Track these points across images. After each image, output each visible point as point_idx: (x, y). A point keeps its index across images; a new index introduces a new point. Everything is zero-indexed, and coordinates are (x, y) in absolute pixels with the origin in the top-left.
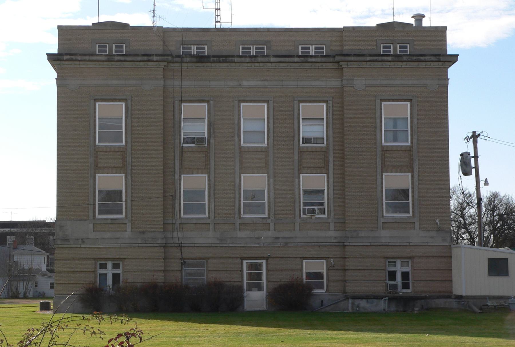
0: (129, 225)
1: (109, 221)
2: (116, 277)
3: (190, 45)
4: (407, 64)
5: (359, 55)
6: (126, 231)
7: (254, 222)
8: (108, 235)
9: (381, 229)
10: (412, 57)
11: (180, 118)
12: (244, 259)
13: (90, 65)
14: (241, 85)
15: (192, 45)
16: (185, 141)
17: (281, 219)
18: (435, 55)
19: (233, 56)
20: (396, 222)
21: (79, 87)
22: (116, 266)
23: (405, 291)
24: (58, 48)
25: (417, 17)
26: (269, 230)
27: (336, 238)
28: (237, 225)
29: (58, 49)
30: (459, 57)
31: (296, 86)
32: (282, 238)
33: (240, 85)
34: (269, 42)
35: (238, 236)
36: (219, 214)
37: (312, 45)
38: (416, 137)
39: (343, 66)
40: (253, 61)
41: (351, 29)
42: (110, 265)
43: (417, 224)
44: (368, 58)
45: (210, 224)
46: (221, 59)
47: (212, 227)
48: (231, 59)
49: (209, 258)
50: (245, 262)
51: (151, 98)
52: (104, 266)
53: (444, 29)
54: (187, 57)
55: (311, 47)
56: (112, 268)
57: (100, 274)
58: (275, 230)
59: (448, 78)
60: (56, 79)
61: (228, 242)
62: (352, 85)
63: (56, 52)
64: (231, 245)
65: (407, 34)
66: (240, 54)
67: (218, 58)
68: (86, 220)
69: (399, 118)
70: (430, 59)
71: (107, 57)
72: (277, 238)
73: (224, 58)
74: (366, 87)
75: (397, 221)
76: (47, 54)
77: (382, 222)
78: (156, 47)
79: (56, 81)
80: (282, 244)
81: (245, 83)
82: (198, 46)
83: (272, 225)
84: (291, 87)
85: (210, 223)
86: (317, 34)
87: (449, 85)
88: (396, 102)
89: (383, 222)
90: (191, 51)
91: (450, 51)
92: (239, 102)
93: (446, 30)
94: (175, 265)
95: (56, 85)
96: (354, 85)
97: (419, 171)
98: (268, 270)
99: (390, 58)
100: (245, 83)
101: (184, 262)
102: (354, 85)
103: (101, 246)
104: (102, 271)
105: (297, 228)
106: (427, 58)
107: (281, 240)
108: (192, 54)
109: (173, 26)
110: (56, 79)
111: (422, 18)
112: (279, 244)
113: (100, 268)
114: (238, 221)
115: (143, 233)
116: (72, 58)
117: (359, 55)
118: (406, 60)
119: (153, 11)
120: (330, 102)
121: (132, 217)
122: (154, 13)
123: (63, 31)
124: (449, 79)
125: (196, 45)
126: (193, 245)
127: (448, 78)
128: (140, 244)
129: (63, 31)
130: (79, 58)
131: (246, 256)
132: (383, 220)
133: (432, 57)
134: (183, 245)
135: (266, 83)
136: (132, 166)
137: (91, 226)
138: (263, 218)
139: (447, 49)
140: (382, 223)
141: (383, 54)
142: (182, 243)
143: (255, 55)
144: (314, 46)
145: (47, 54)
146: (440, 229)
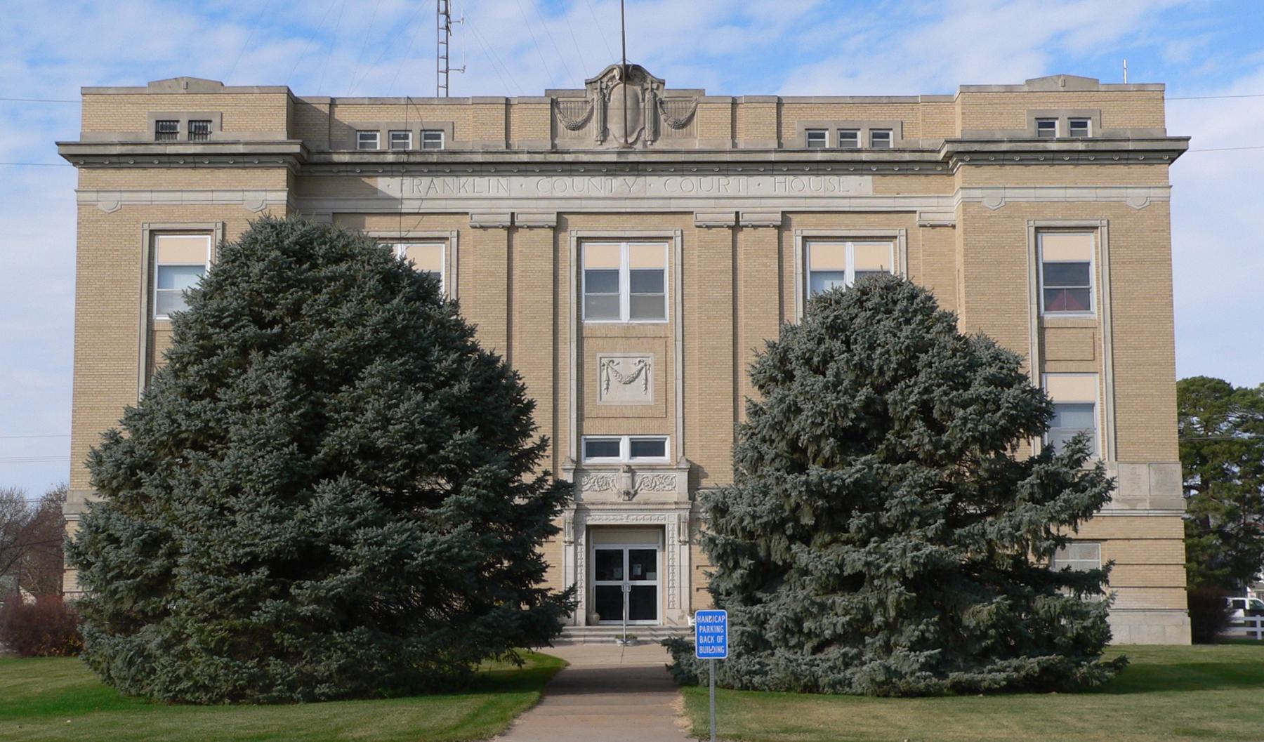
116: (1045, 147)
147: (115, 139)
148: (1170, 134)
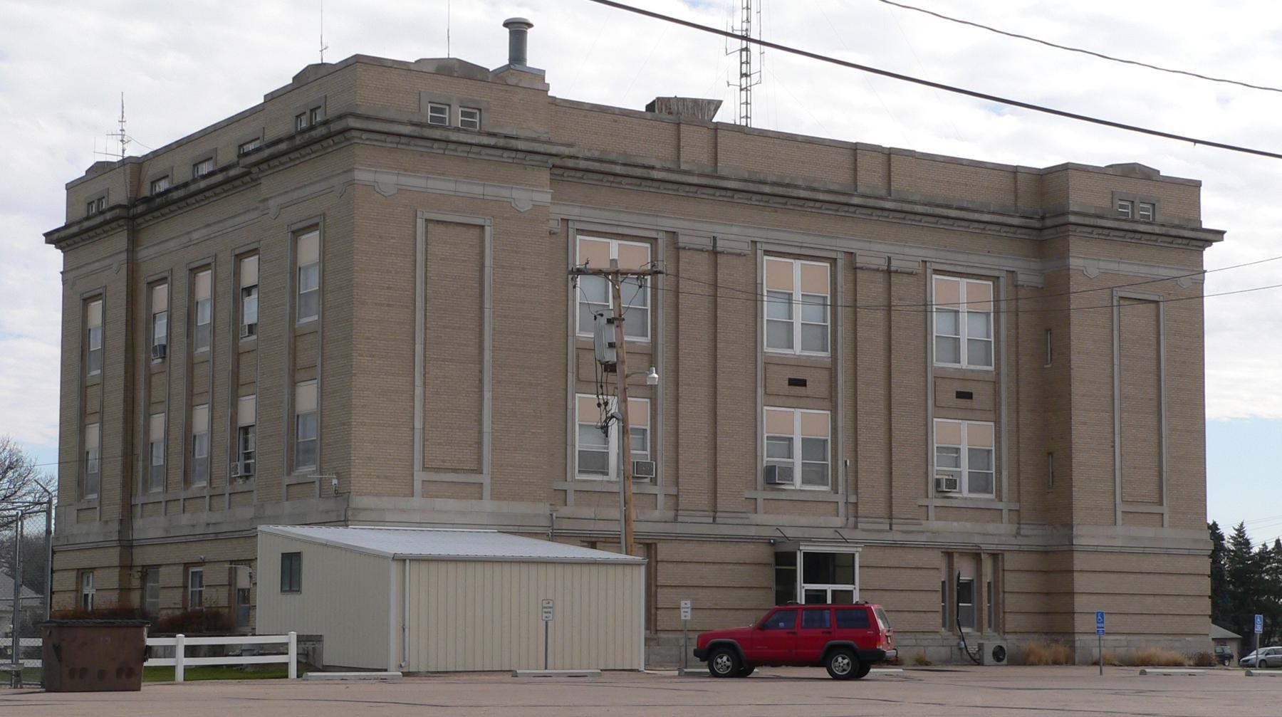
4: (480, 151)
30: (1225, 235)
49: (160, 566)
53: (1198, 184)
59: (1205, 269)
60: (62, 273)
77: (287, 485)
79: (61, 275)
87: (1205, 281)
91: (1207, 224)
93: (1201, 185)
124: (1205, 271)
127: (1205, 269)
132: (287, 481)
139: (1202, 219)
147: (405, 118)
148: (1204, 226)
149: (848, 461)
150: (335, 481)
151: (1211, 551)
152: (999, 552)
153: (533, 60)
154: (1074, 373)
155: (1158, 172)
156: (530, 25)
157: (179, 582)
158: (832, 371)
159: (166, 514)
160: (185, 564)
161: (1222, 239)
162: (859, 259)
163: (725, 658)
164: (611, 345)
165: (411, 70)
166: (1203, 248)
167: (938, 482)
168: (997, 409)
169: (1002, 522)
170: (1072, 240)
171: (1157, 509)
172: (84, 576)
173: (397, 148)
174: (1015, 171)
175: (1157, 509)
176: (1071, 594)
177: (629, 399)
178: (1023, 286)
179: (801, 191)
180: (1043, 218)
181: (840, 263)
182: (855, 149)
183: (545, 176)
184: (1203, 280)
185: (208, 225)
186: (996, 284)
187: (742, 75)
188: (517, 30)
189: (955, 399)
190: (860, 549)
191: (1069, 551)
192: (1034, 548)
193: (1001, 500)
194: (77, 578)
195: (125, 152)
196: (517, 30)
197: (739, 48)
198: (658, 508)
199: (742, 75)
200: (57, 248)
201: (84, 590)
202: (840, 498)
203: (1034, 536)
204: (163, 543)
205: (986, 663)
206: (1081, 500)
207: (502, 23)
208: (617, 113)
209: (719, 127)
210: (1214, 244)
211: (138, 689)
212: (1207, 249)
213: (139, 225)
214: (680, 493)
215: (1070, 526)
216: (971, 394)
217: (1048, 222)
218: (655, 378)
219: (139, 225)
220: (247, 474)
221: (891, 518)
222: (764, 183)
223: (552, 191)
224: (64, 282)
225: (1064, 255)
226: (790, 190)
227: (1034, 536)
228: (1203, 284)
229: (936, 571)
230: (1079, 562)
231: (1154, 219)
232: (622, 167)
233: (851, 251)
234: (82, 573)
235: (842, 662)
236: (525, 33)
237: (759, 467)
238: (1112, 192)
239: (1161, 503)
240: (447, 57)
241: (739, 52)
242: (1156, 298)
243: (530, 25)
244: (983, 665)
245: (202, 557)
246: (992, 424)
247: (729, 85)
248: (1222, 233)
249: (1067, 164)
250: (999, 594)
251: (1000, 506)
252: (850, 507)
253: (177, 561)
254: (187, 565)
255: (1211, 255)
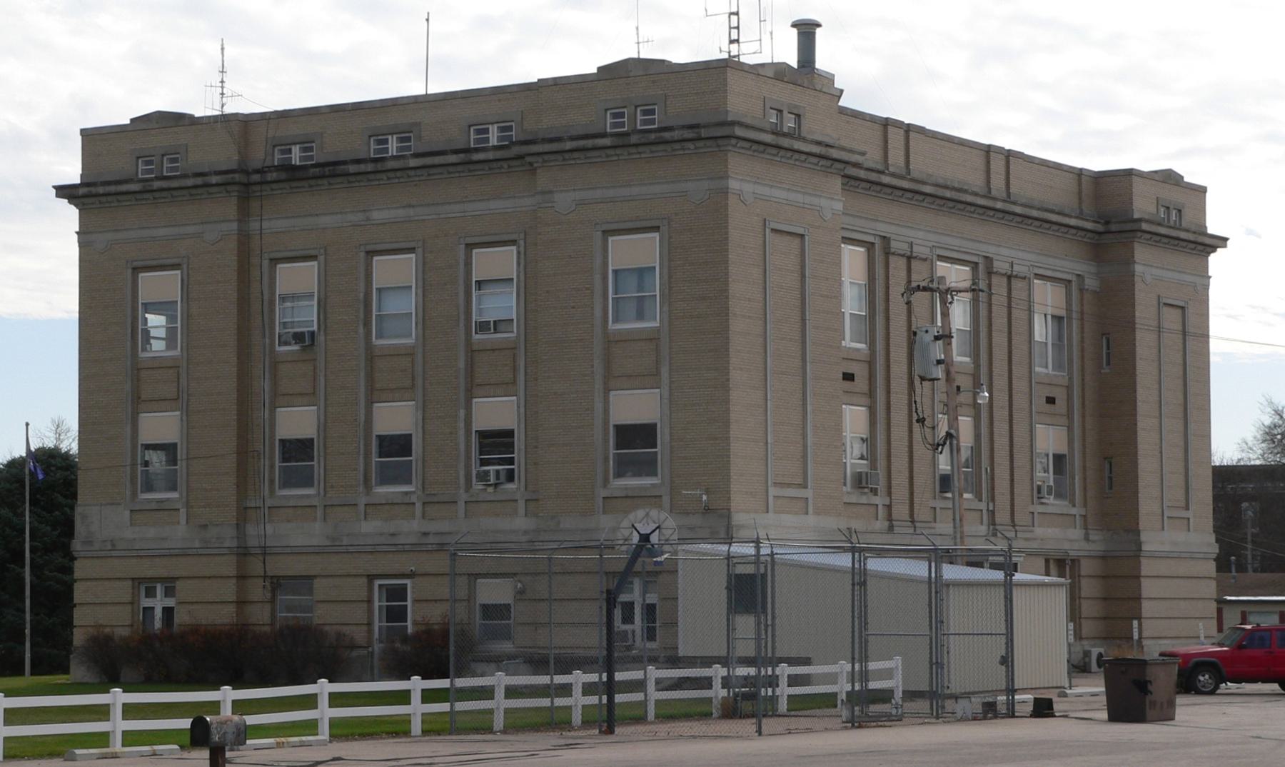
0: (183, 511)
1: (154, 506)
2: (168, 612)
3: (290, 144)
5: (551, 140)
6: (178, 523)
7: (390, 502)
8: (151, 532)
9: (601, 513)
10: (646, 135)
11: (273, 292)
12: (374, 579)
13: (124, 201)
14: (370, 220)
15: (390, 134)
16: (282, 340)
17: (434, 494)
18: (691, 127)
19: (344, 163)
20: (627, 497)
21: (710, 194)
22: (169, 592)
23: (650, 645)
24: (80, 172)
25: (804, 27)
26: (413, 516)
27: (526, 532)
28: (362, 508)
29: (82, 176)
30: (1228, 242)
31: (463, 214)
32: (434, 534)
33: (368, 219)
34: (418, 124)
35: (362, 531)
36: (332, 487)
37: (492, 124)
38: (871, 296)
39: (535, 165)
40: (380, 169)
41: (550, 83)
42: (159, 589)
43: (666, 500)
44: (569, 145)
45: (315, 506)
46: (327, 169)
47: (319, 512)
48: (342, 167)
49: (315, 577)
50: (377, 582)
51: (218, 259)
52: (150, 593)
54: (271, 172)
55: (490, 127)
56: (163, 595)
57: (144, 608)
58: (423, 517)
60: (77, 233)
61: (344, 543)
62: (550, 205)
63: (78, 181)
64: (351, 549)
65: (654, 82)
66: (470, 146)
67: (321, 169)
68: (119, 504)
69: (150, 303)
70: (682, 135)
71: (142, 184)
72: (425, 534)
73: (331, 168)
74: (576, 205)
75: (630, 495)
76: (54, 187)
77: (604, 498)
78: (223, 155)
79: (76, 236)
80: (434, 546)
81: (377, 215)
82: (302, 146)
83: (419, 506)
84: (454, 215)
85: (318, 504)
86: (499, 100)
88: (633, 234)
89: (604, 496)
90: (487, 136)
91: (1211, 230)
92: (604, 235)
94: (257, 591)
95: (77, 244)
96: (554, 204)
97: (671, 382)
98: (370, 601)
99: (606, 142)
100: (377, 215)
101: (276, 584)
102: (554, 204)
103: (142, 553)
104: (147, 603)
105: (522, 511)
106: (676, 134)
107: (431, 539)
108: (293, 163)
109: (214, 111)
110: (77, 233)
111: (815, 29)
112: (430, 547)
113: (146, 597)
114: (363, 500)
115: (205, 527)
116: (91, 192)
117: (551, 140)
118: (638, 142)
119: (220, 85)
120: (522, 243)
121: (188, 495)
122: (222, 87)
123: (93, 139)
125: (396, 133)
126: (288, 550)
128: (198, 550)
129: (93, 139)
130: (101, 190)
131: (379, 572)
132: (604, 493)
133: (685, 132)
134: (268, 551)
135: (411, 212)
136: (188, 395)
137: (127, 513)
138: (406, 493)
140: (601, 499)
141: (376, 156)
142: (265, 547)
143: (395, 154)
144: (496, 126)
145: (54, 187)
146: (709, 509)
149: (989, 469)
150: (705, 497)
151: (1216, 555)
152: (1076, 558)
153: (823, 62)
154: (1138, 379)
155: (1182, 177)
156: (819, 25)
157: (363, 594)
158: (871, 363)
159: (325, 519)
160: (368, 576)
161: (1225, 246)
162: (996, 264)
163: (1207, 676)
164: (939, 362)
165: (758, 75)
166: (1209, 253)
167: (1039, 489)
168: (1070, 415)
169: (1075, 528)
170: (1136, 245)
171: (1184, 514)
172: (141, 586)
173: (781, 162)
174: (1080, 173)
175: (1184, 514)
176: (1138, 599)
177: (960, 418)
178: (1087, 290)
179: (968, 196)
180: (1107, 223)
181: (981, 267)
182: (988, 151)
183: (838, 182)
184: (1209, 285)
185: (410, 206)
186: (1068, 287)
187: (732, 42)
188: (807, 31)
189: (842, 381)
190: (1022, 559)
191: (1136, 552)
192: (1092, 553)
193: (1074, 506)
194: (133, 588)
195: (224, 107)
196: (807, 31)
197: (729, 11)
198: (879, 518)
199: (732, 42)
200: (70, 202)
201: (141, 603)
202: (983, 506)
203: (1098, 543)
204: (860, 577)
205: (1093, 671)
206: (1147, 504)
207: (790, 24)
208: (868, 119)
209: (911, 129)
210: (1218, 249)
211: (1171, 718)
212: (1212, 255)
213: (254, 192)
214: (893, 504)
215: (1138, 533)
216: (853, 375)
217: (1114, 227)
218: (986, 397)
219: (254, 192)
220: (498, 482)
221: (913, 522)
222: (965, 191)
223: (844, 199)
224: (82, 245)
225: (1129, 261)
226: (961, 194)
227: (1098, 543)
228: (1208, 289)
229: (29, 427)
230: (1147, 567)
231: (1181, 225)
232: (866, 172)
233: (988, 255)
234: (139, 583)
235: (1204, 678)
236: (813, 34)
237: (937, 475)
238: (1157, 198)
239: (1187, 508)
240: (770, 61)
241: (727, 15)
242: (801, 231)
243: (819, 25)
244: (1090, 672)
245: (413, 568)
246: (1066, 428)
247: (721, 51)
248: (1226, 240)
249: (1132, 170)
250: (1075, 600)
251: (1074, 511)
252: (990, 513)
253: (361, 571)
254: (370, 577)
255: (1216, 261)
